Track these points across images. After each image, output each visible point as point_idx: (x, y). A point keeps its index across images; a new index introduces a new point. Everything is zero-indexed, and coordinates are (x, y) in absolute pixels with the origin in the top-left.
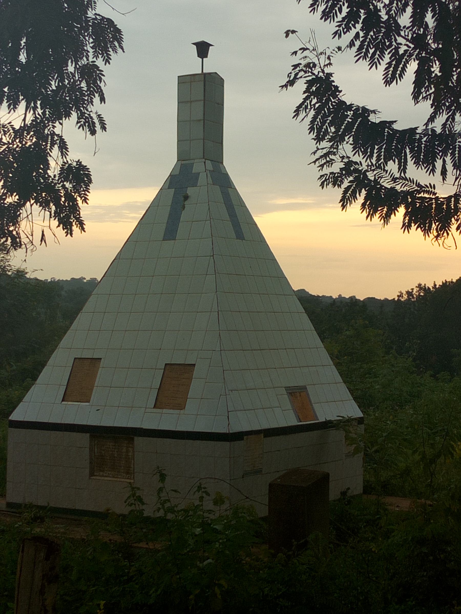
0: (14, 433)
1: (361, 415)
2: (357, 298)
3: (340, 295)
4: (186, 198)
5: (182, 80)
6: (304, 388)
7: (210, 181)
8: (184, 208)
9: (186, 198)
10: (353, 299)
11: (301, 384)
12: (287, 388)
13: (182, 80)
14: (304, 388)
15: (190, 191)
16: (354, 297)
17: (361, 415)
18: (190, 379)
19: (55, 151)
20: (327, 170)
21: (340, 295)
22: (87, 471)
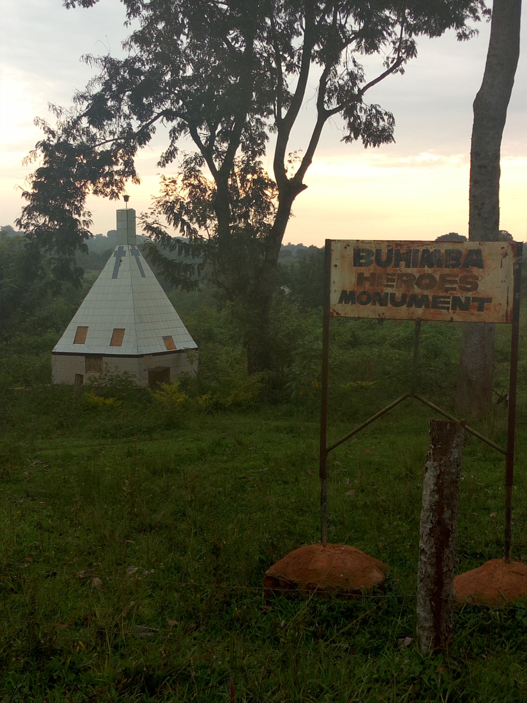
0: (54, 356)
1: (197, 347)
2: (304, 245)
3: (289, 243)
4: (121, 261)
5: (118, 211)
6: (171, 337)
7: (131, 254)
8: (120, 265)
9: (121, 261)
10: (300, 245)
11: (169, 335)
12: (163, 337)
13: (118, 211)
14: (171, 337)
15: (122, 258)
16: (302, 244)
17: (197, 347)
18: (123, 334)
19: (72, 263)
20: (159, 271)
21: (289, 243)
22: (85, 371)
